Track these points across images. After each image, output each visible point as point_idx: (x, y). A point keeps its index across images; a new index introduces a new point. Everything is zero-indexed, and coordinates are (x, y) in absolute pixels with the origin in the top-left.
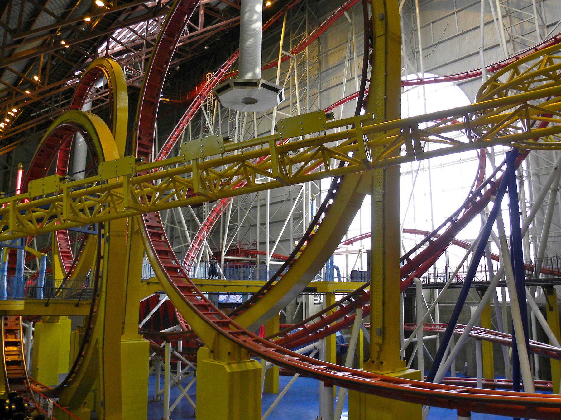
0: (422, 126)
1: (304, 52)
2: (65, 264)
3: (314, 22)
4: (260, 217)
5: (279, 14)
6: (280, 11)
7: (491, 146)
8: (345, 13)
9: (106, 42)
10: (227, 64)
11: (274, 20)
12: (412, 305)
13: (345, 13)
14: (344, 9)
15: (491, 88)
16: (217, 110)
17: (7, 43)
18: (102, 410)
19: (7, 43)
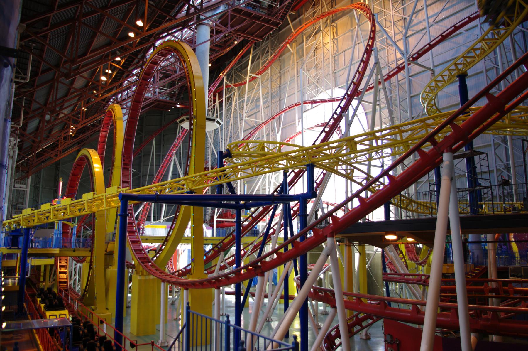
0: (356, 139)
1: (267, 73)
2: (128, 229)
3: (274, 46)
4: (160, 324)
5: (248, 45)
6: (248, 44)
7: (323, 242)
8: (288, 46)
9: (121, 94)
10: (215, 83)
11: (245, 51)
12: (468, 297)
13: (288, 46)
14: (287, 43)
15: (235, 271)
16: (217, 113)
17: (58, 98)
18: (451, 249)
19: (58, 98)
